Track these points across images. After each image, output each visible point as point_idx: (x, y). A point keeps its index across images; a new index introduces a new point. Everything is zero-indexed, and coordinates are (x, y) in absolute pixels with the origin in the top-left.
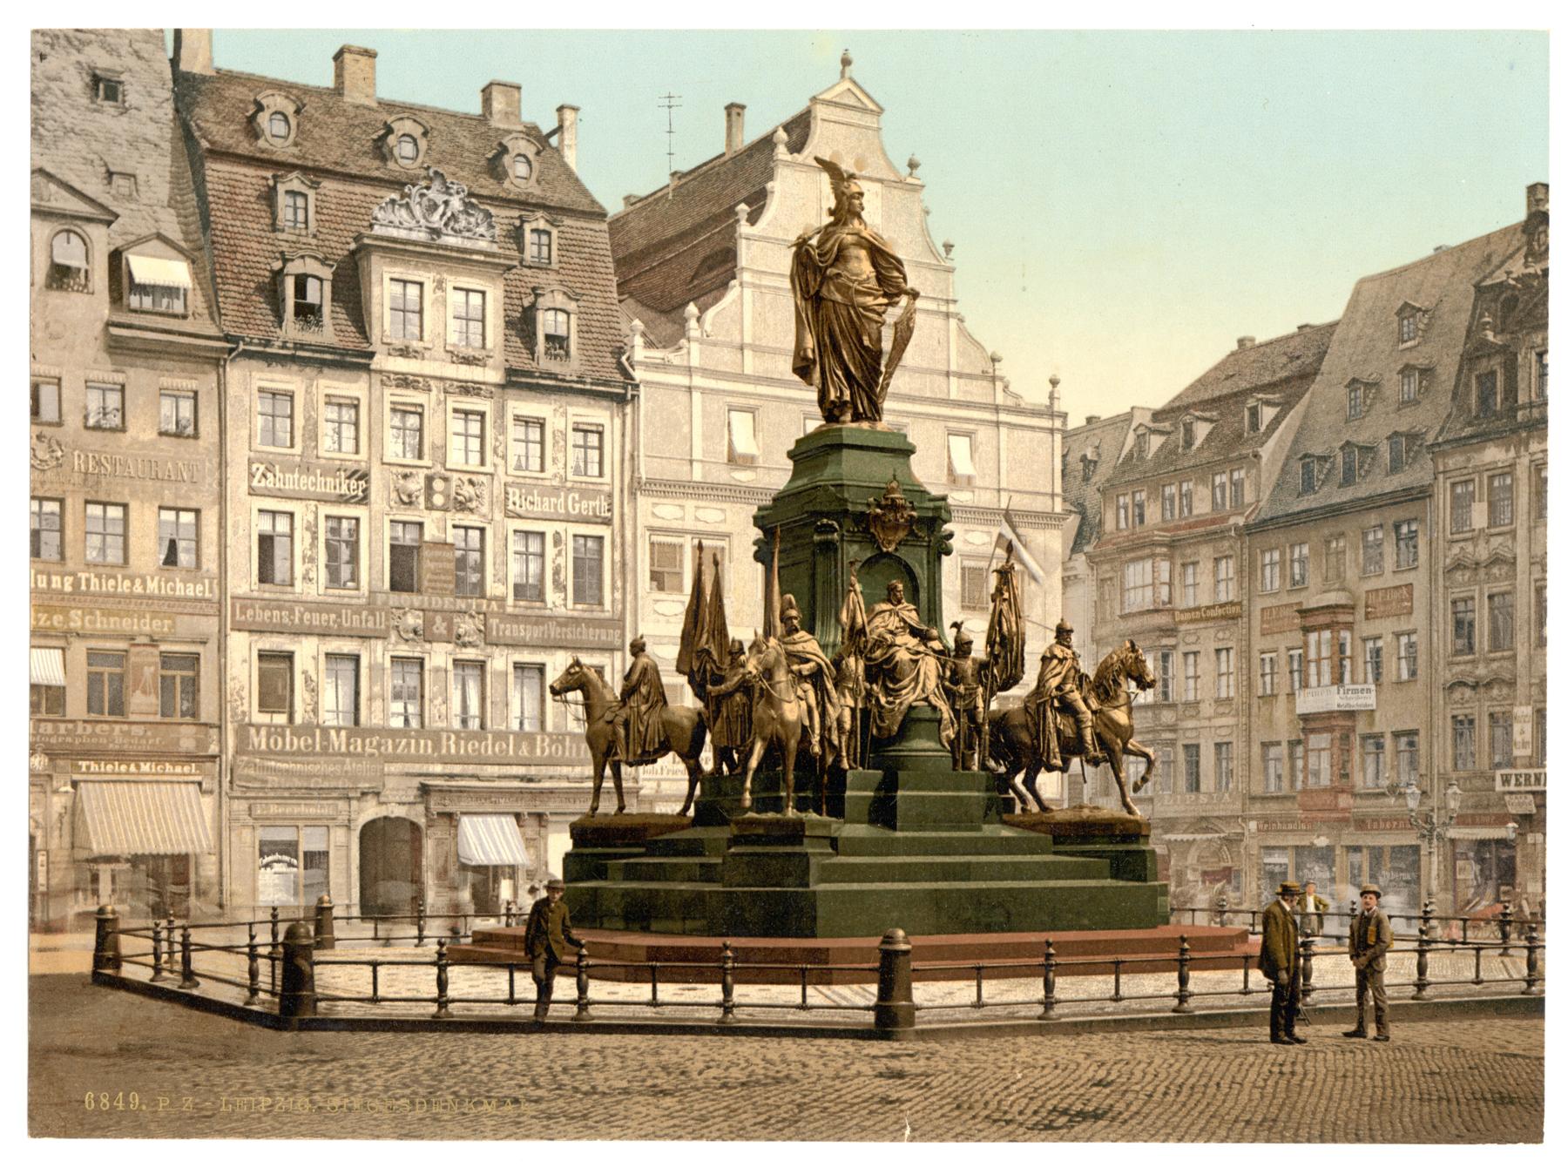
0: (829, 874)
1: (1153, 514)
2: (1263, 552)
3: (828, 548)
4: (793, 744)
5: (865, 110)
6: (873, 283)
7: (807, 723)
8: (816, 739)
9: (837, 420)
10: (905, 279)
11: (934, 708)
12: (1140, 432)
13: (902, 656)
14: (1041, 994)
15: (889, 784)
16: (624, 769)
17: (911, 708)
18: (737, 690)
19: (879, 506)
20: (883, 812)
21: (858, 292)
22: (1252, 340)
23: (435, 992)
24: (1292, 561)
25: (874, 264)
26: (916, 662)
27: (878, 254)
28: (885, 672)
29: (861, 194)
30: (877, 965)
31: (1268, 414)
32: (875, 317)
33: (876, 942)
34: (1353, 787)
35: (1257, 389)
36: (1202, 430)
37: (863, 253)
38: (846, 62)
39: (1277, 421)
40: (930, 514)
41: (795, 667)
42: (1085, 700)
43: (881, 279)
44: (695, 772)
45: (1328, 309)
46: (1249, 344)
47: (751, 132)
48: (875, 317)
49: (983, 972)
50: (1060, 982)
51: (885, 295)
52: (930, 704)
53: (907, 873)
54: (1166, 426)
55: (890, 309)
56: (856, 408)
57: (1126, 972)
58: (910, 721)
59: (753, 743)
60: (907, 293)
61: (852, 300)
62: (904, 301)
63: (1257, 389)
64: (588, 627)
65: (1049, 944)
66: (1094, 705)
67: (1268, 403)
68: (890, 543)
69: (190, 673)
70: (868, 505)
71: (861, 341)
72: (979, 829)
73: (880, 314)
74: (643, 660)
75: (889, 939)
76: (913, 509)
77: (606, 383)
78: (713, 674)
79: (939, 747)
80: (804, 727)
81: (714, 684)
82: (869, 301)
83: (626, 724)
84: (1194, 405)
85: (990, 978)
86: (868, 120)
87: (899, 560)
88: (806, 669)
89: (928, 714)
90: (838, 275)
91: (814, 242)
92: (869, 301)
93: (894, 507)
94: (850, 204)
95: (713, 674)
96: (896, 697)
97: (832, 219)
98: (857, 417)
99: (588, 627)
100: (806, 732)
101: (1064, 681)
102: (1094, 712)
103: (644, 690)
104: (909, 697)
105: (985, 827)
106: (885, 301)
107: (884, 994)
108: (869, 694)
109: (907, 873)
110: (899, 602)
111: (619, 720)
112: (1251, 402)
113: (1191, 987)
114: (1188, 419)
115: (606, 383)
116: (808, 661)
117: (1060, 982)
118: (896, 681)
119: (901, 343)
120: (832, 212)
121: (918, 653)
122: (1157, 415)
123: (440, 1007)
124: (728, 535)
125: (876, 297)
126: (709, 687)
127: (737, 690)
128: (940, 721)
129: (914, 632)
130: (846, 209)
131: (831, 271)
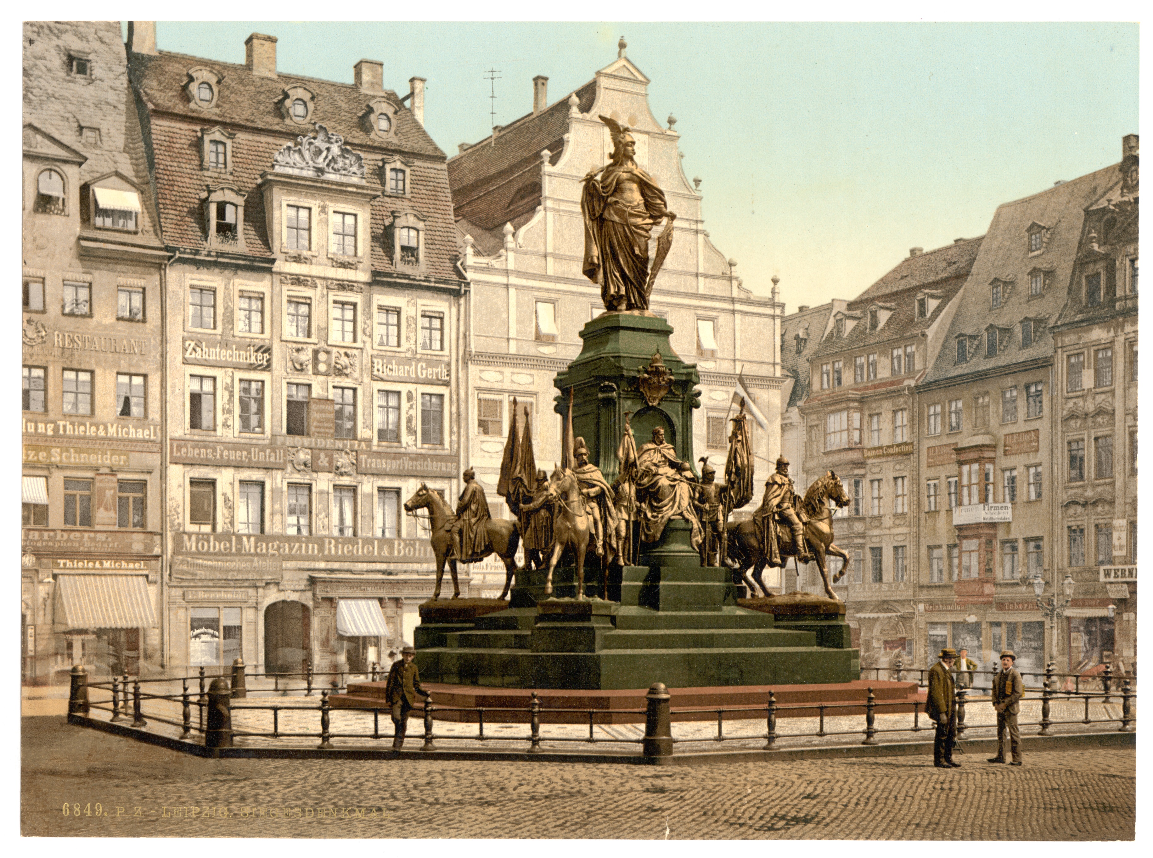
3: (609, 403)
4: (583, 547)
5: (636, 81)
6: (642, 208)
8: (600, 543)
9: (615, 309)
10: (665, 205)
11: (687, 521)
12: (839, 317)
13: (664, 482)
14: (765, 731)
16: (459, 566)
17: (670, 520)
19: (646, 372)
21: (631, 215)
24: (950, 412)
25: (643, 194)
27: (646, 187)
28: (651, 494)
29: (633, 143)
31: (932, 304)
32: (644, 233)
36: (884, 316)
37: (635, 186)
42: (798, 515)
43: (648, 205)
45: (976, 227)
46: (918, 253)
48: (644, 233)
51: (651, 217)
52: (684, 518)
53: (667, 642)
54: (858, 313)
55: (655, 228)
56: (629, 300)
60: (667, 215)
62: (665, 221)
66: (805, 518)
67: (932, 296)
68: (654, 399)
70: (639, 371)
71: (633, 251)
72: (720, 610)
73: (647, 231)
74: (473, 486)
75: (654, 690)
77: (446, 282)
78: (524, 495)
79: (690, 549)
80: (591, 535)
82: (639, 221)
83: (461, 532)
84: (878, 298)
86: (638, 88)
87: (661, 412)
88: (593, 491)
89: (683, 525)
91: (599, 178)
92: (639, 221)
94: (625, 150)
95: (524, 495)
96: (659, 512)
97: (612, 161)
98: (630, 307)
99: (432, 461)
100: (593, 538)
101: (783, 501)
102: (804, 524)
103: (473, 507)
105: (725, 608)
107: (651, 730)
108: (639, 510)
109: (667, 642)
110: (661, 443)
111: (456, 529)
112: (920, 296)
114: (873, 308)
115: (446, 282)
118: (659, 501)
120: (611, 156)
121: (675, 480)
122: (851, 305)
126: (521, 505)
128: (691, 530)
129: (672, 465)
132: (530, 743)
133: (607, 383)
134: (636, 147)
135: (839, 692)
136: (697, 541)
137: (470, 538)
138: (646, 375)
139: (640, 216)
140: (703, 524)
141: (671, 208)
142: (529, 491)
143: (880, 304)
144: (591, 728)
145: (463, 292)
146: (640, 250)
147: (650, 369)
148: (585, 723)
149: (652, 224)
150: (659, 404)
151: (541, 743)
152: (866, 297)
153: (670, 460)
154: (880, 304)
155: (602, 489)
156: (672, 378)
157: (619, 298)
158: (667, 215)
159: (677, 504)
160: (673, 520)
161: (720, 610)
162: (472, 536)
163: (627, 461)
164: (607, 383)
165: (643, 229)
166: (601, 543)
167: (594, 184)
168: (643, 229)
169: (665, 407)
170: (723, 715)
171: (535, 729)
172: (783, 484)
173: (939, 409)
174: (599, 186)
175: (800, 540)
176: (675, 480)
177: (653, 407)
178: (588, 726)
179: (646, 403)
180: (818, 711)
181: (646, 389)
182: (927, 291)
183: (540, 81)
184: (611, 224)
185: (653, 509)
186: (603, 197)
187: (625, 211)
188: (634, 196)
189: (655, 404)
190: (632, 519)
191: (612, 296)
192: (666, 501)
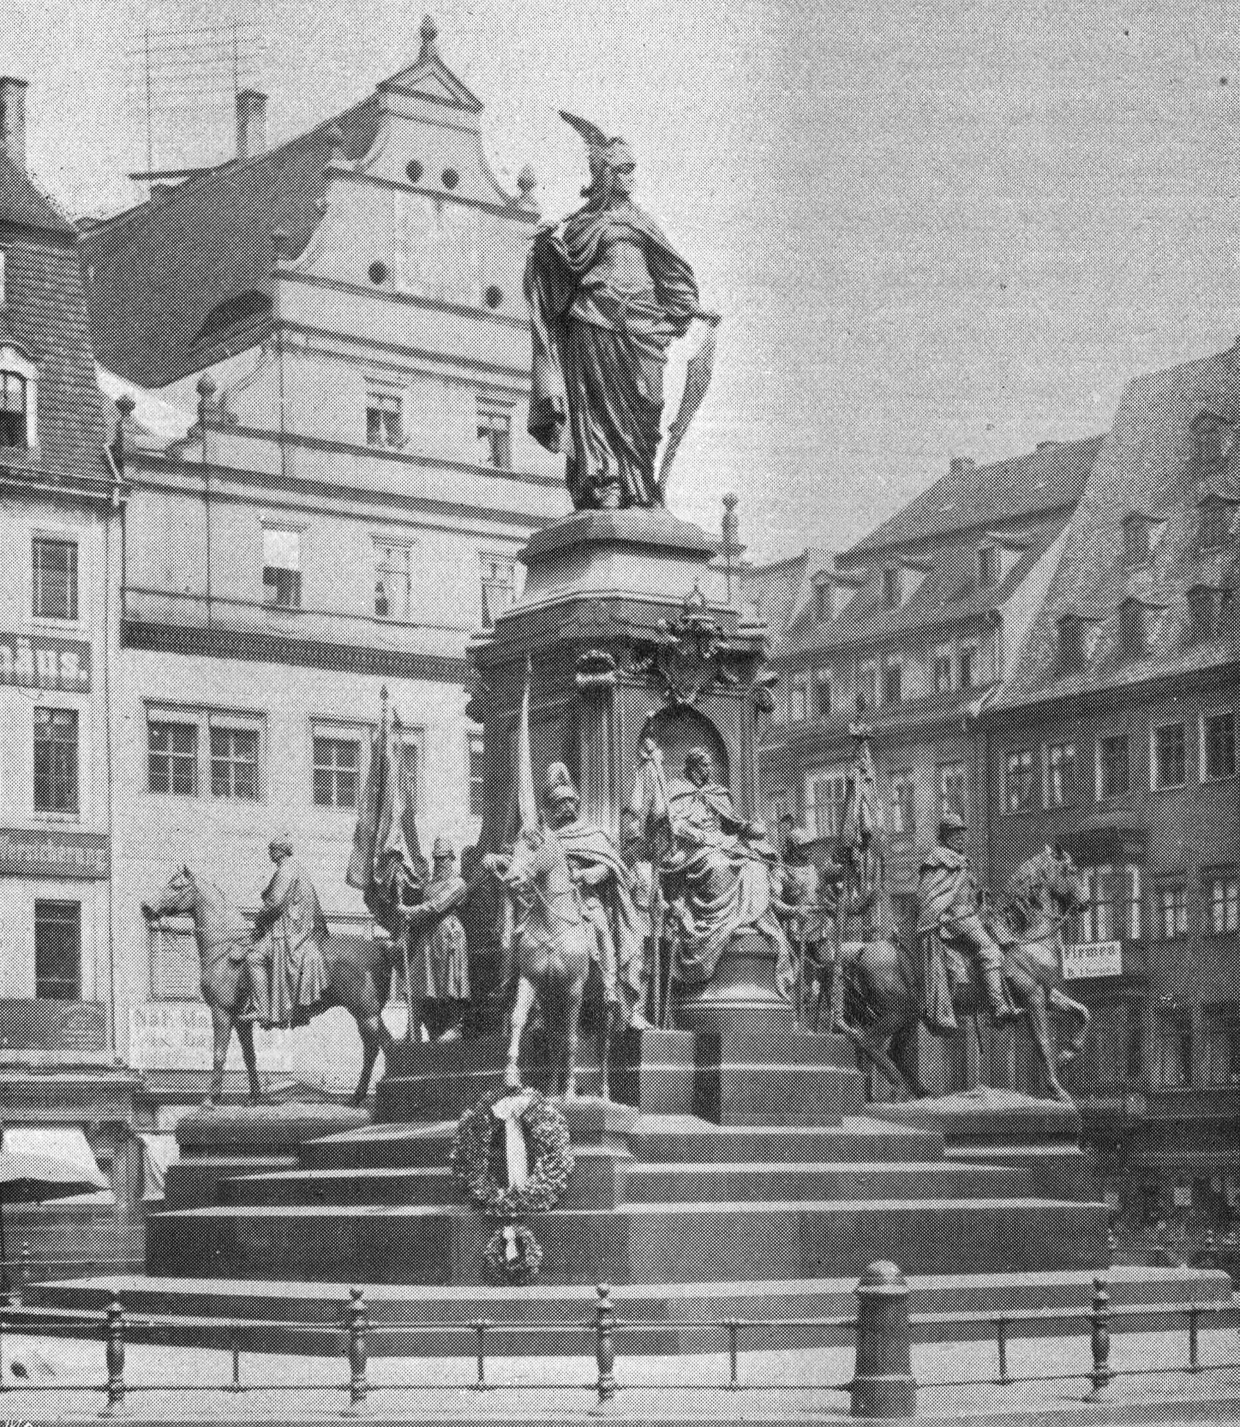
0: (640, 1189)
1: (842, 702)
2: (1051, 747)
3: (599, 697)
4: (577, 988)
5: (456, 104)
6: (651, 300)
7: (597, 958)
8: (609, 981)
9: (597, 504)
10: (696, 295)
11: (769, 938)
12: (821, 581)
13: (718, 862)
14: (1087, 1363)
15: (708, 1047)
16: (257, 1032)
17: (735, 937)
18: (447, 912)
19: (673, 631)
20: (705, 1098)
21: (631, 313)
22: (970, 462)
23: (102, 1378)
24: (1051, 768)
25: (652, 272)
26: (736, 870)
27: (658, 257)
28: (688, 884)
29: (631, 166)
30: (853, 1318)
31: (1007, 559)
32: (656, 352)
33: (849, 1285)
34: (1147, 1083)
35: (1000, 524)
36: (910, 581)
37: (635, 253)
38: (428, 34)
39: (1018, 574)
40: (746, 647)
41: (577, 873)
42: (988, 929)
43: (663, 296)
44: (373, 1039)
45: (1088, 417)
46: (965, 466)
47: (281, 126)
48: (656, 352)
49: (1201, 1319)
50: (1117, 1341)
51: (669, 318)
52: (761, 933)
53: (742, 1188)
54: (857, 572)
55: (675, 341)
56: (624, 488)
57: (1204, 1327)
58: (731, 962)
59: (513, 987)
60: (702, 317)
61: (620, 322)
62: (696, 325)
63: (1000, 524)
64: (57, 844)
65: (1099, 1286)
66: (1005, 936)
67: (1009, 545)
68: (689, 689)
69: (232, 742)
70: (658, 630)
71: (634, 387)
72: (838, 1123)
73: (660, 347)
74: (288, 870)
75: (871, 1278)
76: (722, 638)
77: (83, 483)
78: (407, 889)
79: (777, 997)
80: (593, 964)
81: (406, 903)
82: (644, 326)
83: (268, 964)
84: (896, 546)
85: (758, 1346)
86: (461, 117)
87: (697, 716)
88: (594, 875)
89: (758, 945)
90: (600, 285)
91: (559, 234)
92: (644, 326)
93: (699, 635)
94: (616, 179)
95: (407, 889)
96: (709, 921)
97: (584, 201)
98: (626, 502)
99: (57, 844)
100: (595, 968)
101: (957, 901)
102: (1005, 948)
103: (294, 912)
104: (729, 922)
105: (845, 1120)
106: (668, 327)
107: (865, 1364)
108: (669, 914)
109: (742, 1188)
110: (705, 781)
111: (255, 957)
112: (984, 544)
113: (1113, 1362)
114: (890, 564)
115: (83, 483)
116: (590, 864)
117: (1117, 1341)
118: (708, 897)
119: (694, 394)
120: (585, 193)
121: (738, 856)
122: (843, 560)
123: (112, 1399)
124: (260, 715)
125: (657, 321)
126: (402, 907)
127: (447, 912)
128: (774, 958)
129: (728, 827)
130: (605, 190)
131: (590, 278)
132: (104, 1396)
133: (594, 653)
134: (636, 174)
135: (988, 1291)
136: (786, 980)
137: (288, 976)
138: (674, 639)
139: (644, 316)
140: (795, 945)
141: (705, 303)
142: (414, 879)
143: (905, 558)
144: (734, 1359)
145: (116, 503)
146: (648, 385)
147: (681, 626)
148: (471, 1354)
149: (672, 334)
150: (696, 701)
151: (371, 1395)
152: (870, 545)
153: (722, 818)
154: (905, 558)
155: (611, 870)
156: (724, 645)
157: (603, 481)
158: (702, 317)
159: (745, 905)
160: (740, 936)
161: (838, 1123)
162: (293, 971)
163: (650, 816)
164: (594, 653)
165: (650, 342)
166: (613, 980)
167: (551, 247)
168: (650, 342)
169: (709, 708)
170: (1009, 1328)
171: (605, 1366)
172: (958, 869)
173: (1027, 760)
174: (563, 251)
175: (995, 981)
176: (738, 856)
177: (687, 709)
178: (474, 1360)
179: (672, 699)
180: (996, 1328)
181: (672, 667)
182: (998, 535)
183: (249, 103)
184: (588, 332)
185: (698, 913)
186: (570, 273)
187: (617, 304)
188: (626, 273)
189: (690, 699)
190: (659, 934)
191: (592, 478)
192: (721, 900)
